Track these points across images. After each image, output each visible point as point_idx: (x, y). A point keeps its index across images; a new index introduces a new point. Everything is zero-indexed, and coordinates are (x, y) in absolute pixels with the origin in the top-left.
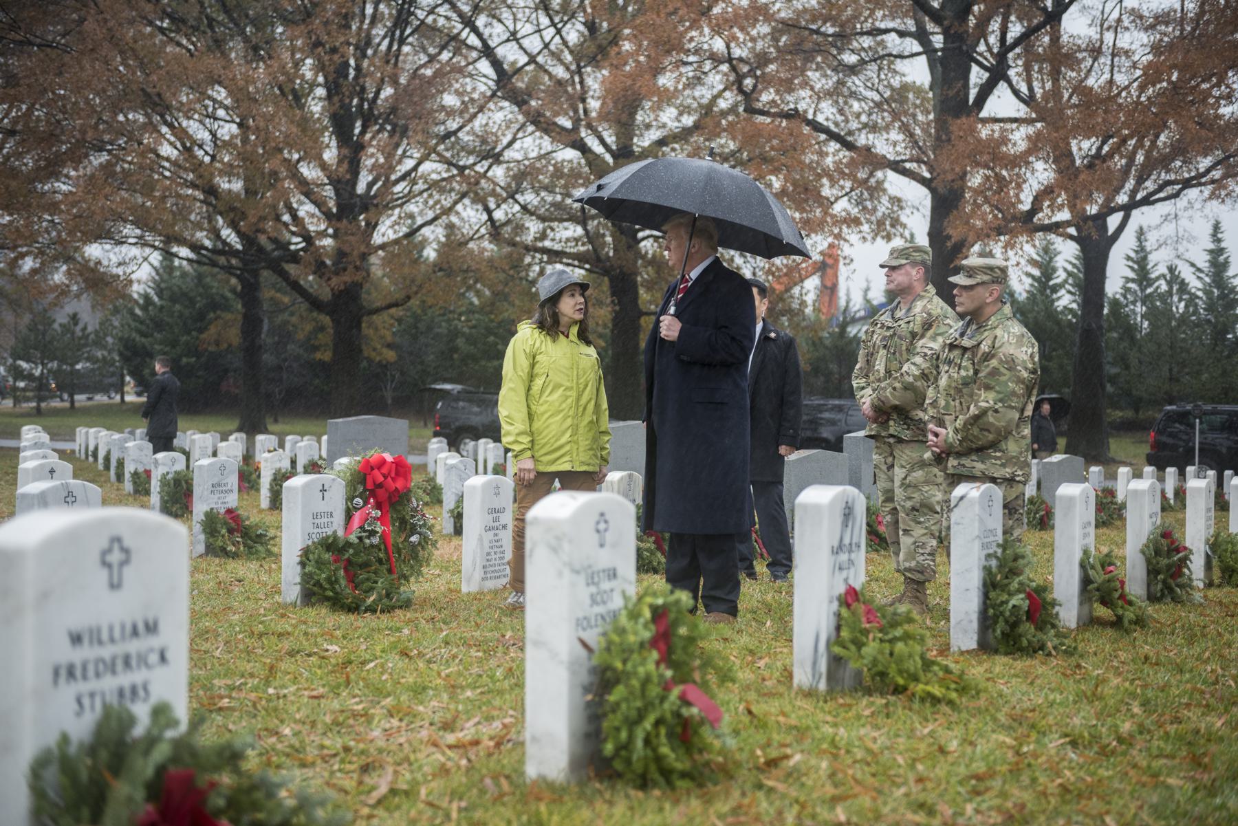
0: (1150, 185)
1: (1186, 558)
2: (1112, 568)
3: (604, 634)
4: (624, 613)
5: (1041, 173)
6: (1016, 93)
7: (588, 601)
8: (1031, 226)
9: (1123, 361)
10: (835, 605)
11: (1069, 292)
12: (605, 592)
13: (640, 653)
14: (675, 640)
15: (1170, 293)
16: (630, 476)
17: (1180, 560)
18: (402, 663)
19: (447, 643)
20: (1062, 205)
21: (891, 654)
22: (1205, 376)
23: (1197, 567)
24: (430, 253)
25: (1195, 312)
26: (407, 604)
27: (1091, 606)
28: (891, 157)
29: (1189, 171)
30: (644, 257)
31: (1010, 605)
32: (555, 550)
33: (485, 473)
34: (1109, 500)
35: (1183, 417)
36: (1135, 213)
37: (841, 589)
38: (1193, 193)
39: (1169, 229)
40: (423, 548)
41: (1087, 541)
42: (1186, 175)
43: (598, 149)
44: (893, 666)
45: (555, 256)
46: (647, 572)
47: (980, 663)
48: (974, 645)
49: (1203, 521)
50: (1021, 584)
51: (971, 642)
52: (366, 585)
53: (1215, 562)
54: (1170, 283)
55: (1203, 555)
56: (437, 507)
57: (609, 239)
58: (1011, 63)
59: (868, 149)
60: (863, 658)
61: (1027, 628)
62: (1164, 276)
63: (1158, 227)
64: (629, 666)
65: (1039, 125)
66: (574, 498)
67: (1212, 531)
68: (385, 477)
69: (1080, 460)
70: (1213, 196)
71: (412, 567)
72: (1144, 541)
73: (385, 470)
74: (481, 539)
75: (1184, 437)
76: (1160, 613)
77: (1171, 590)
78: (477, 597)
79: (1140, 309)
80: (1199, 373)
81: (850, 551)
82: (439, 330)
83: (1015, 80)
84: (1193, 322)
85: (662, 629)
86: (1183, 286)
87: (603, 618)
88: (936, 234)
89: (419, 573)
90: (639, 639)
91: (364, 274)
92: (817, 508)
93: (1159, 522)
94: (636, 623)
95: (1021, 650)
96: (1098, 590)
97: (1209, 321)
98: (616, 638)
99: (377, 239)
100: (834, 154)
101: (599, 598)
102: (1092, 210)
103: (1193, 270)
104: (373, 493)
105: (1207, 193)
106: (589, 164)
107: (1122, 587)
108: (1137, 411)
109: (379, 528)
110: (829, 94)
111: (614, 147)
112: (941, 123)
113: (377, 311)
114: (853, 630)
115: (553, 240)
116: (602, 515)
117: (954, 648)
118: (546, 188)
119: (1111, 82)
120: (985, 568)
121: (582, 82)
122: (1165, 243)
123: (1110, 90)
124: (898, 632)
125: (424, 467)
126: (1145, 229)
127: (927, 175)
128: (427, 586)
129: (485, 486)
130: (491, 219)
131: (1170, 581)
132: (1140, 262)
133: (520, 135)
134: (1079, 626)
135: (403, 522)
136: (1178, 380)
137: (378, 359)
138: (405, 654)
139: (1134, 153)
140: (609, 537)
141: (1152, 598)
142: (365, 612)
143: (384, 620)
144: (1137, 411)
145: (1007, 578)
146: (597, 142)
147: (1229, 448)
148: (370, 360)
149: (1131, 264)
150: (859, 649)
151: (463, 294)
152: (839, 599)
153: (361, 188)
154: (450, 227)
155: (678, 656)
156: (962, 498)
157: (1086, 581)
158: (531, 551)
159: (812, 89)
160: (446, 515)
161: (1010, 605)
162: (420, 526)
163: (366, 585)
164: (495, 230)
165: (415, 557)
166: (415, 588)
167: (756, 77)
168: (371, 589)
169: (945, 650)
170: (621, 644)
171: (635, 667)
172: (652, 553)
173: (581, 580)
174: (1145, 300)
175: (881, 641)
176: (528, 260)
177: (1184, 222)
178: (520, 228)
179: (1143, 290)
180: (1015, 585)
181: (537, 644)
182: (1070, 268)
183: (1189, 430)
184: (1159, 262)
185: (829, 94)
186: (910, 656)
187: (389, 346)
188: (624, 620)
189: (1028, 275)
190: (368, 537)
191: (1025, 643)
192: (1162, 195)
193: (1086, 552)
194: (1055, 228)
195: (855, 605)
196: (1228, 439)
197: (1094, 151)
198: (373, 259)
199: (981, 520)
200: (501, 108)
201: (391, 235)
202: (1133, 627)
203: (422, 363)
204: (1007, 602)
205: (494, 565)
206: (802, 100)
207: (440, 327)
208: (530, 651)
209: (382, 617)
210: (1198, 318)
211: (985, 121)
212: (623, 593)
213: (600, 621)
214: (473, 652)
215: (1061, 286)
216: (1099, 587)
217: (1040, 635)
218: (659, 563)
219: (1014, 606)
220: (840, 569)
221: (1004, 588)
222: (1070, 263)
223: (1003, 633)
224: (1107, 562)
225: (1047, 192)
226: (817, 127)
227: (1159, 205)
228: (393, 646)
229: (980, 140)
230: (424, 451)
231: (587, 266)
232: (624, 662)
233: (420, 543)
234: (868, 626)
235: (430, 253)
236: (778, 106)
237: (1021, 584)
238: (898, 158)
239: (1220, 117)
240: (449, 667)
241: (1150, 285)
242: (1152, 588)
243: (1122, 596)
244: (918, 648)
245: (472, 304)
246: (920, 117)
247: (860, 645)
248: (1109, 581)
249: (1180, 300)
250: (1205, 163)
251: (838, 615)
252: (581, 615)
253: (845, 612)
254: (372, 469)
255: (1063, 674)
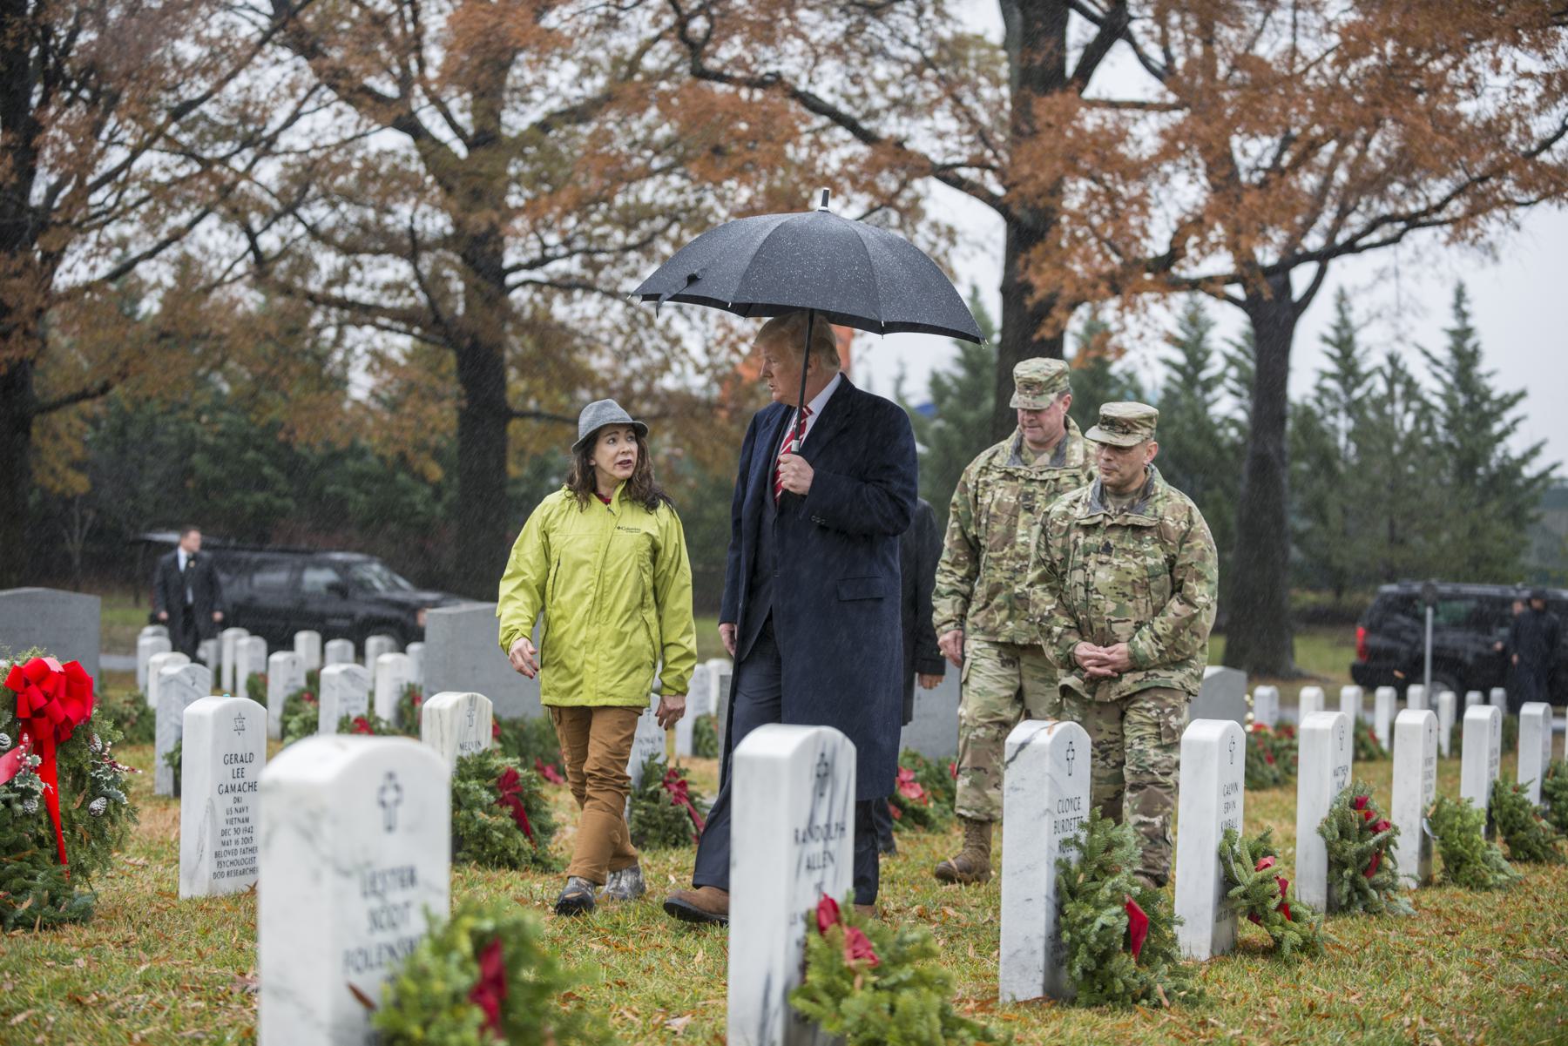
0: (1356, 221)
1: (1386, 844)
2: (1268, 860)
3: (392, 979)
4: (427, 943)
5: (1184, 191)
6: (1144, 60)
7: (365, 923)
8: (1163, 277)
9: (1317, 509)
10: (800, 928)
11: (1233, 392)
12: (396, 908)
13: (452, 1012)
14: (514, 990)
15: (1390, 397)
16: (472, 701)
17: (1379, 844)
18: (71, 1017)
19: (147, 985)
20: (1218, 244)
21: (892, 1010)
22: (1445, 537)
23: (1406, 857)
24: (150, 305)
25: (1430, 432)
26: (84, 916)
27: (1235, 922)
28: (938, 159)
29: (1416, 200)
30: (516, 317)
31: (1097, 925)
32: (308, 835)
33: (234, 693)
34: (1285, 742)
35: (1407, 604)
36: (1334, 265)
37: (811, 902)
38: (1421, 237)
39: (1386, 293)
40: (113, 821)
41: (1230, 815)
42: (1412, 208)
43: (443, 133)
44: (894, 1029)
45: (363, 313)
46: (499, 865)
47: (1045, 1022)
48: (1037, 991)
49: (1420, 778)
50: (1115, 889)
51: (1031, 986)
52: (16, 883)
53: (1435, 847)
54: (1390, 382)
55: (1418, 836)
56: (147, 747)
57: (458, 286)
58: (1133, 12)
59: (899, 144)
60: (844, 1017)
61: (1124, 963)
62: (1380, 370)
63: (1369, 288)
64: (433, 1033)
65: (1178, 116)
66: (343, 747)
67: (1432, 796)
68: (49, 698)
69: (1241, 676)
70: (1452, 239)
71: (94, 852)
72: (1325, 814)
73: (48, 687)
74: (212, 809)
75: (1412, 638)
76: (1342, 932)
77: (1364, 894)
78: (204, 906)
79: (1344, 423)
80: (1437, 531)
81: (827, 838)
82: (163, 439)
83: (1140, 39)
84: (1426, 447)
85: (492, 971)
86: (1411, 385)
87: (392, 951)
88: (1012, 291)
89: (106, 863)
90: (449, 988)
91: (39, 344)
92: (771, 764)
93: (1348, 782)
94: (446, 960)
95: (1112, 998)
96: (1245, 896)
97: (1450, 446)
98: (412, 987)
99: (62, 280)
100: (842, 150)
101: (384, 919)
102: (1267, 256)
103: (1425, 360)
104: (28, 726)
105: (1443, 237)
106: (424, 158)
107: (1283, 893)
108: (1339, 591)
109: (39, 786)
110: (836, 49)
111: (470, 131)
112: (1022, 106)
113: (55, 406)
114: (828, 970)
115: (360, 284)
116: (391, 776)
117: (1005, 997)
118: (350, 197)
119: (1294, 50)
120: (1058, 862)
121: (415, 19)
122: (1379, 315)
123: (1291, 65)
124: (906, 973)
125: (130, 677)
126: (1348, 290)
127: (998, 190)
128: (123, 885)
129: (219, 715)
130: (254, 247)
131: (1364, 880)
132: (1343, 344)
133: (310, 105)
134: (1213, 956)
135: (79, 774)
136: (1402, 542)
137: (59, 487)
138: (76, 1001)
139: (1331, 168)
140: (403, 814)
141: (1335, 908)
142: (15, 927)
143: (45, 943)
144: (1339, 591)
145: (1094, 879)
146: (439, 118)
147: (1478, 656)
148: (46, 492)
149: (1329, 348)
150: (837, 1002)
151: (205, 377)
152: (807, 918)
153: (37, 194)
154: (185, 262)
155: (520, 1015)
156: (1023, 746)
157: (1227, 881)
158: (269, 835)
159: (804, 37)
160: (160, 763)
161: (1097, 925)
162: (108, 784)
163: (16, 883)
164: (261, 264)
165: (102, 834)
166: (100, 888)
167: (710, 18)
168: (25, 889)
169: (987, 1003)
170: (420, 996)
171: (442, 1034)
172: (508, 833)
173: (354, 886)
174: (1354, 408)
175: (876, 987)
176: (317, 319)
177: (1407, 282)
178: (305, 265)
179: (1348, 392)
180: (1105, 892)
181: (278, 993)
182: (1231, 351)
183: (1417, 625)
184: (1372, 350)
185: (836, 49)
186: (923, 1013)
187: (78, 466)
188: (425, 956)
189: (1167, 362)
190: (21, 801)
191: (1119, 986)
192: (1375, 237)
193: (1228, 835)
194: (1208, 284)
195: (832, 929)
196: (1476, 641)
197: (1267, 162)
198: (54, 315)
199: (1054, 783)
200: (278, 62)
201: (82, 274)
202: (1298, 955)
203: (134, 495)
204: (1091, 920)
205: (235, 852)
206: (790, 61)
207: (165, 433)
208: (265, 1004)
209: (43, 936)
210: (1435, 441)
211: (1092, 104)
212: (426, 911)
213: (386, 954)
214: (190, 1001)
215: (1219, 379)
216: (1248, 897)
217: (1145, 973)
218: (520, 851)
219: (1104, 927)
220: (808, 867)
221: (1088, 896)
222: (1232, 343)
223: (1084, 971)
224: (1261, 852)
225: (1193, 225)
226: (813, 104)
227: (1368, 254)
228: (57, 987)
229: (1080, 132)
230: (131, 648)
231: (417, 330)
232: (426, 1025)
233: (106, 813)
234: (853, 963)
235: (150, 305)
236: (746, 67)
237: (1115, 889)
238: (950, 161)
239: (1458, 117)
240: (148, 1023)
241: (1358, 383)
242: (1335, 892)
243: (1283, 907)
244: (936, 1000)
245: (219, 393)
246: (987, 93)
247: (837, 995)
248: (1263, 881)
249: (1407, 410)
250: (1439, 189)
251: (804, 945)
252: (352, 945)
253: (815, 941)
254: (27, 683)
255: (1180, 1038)
